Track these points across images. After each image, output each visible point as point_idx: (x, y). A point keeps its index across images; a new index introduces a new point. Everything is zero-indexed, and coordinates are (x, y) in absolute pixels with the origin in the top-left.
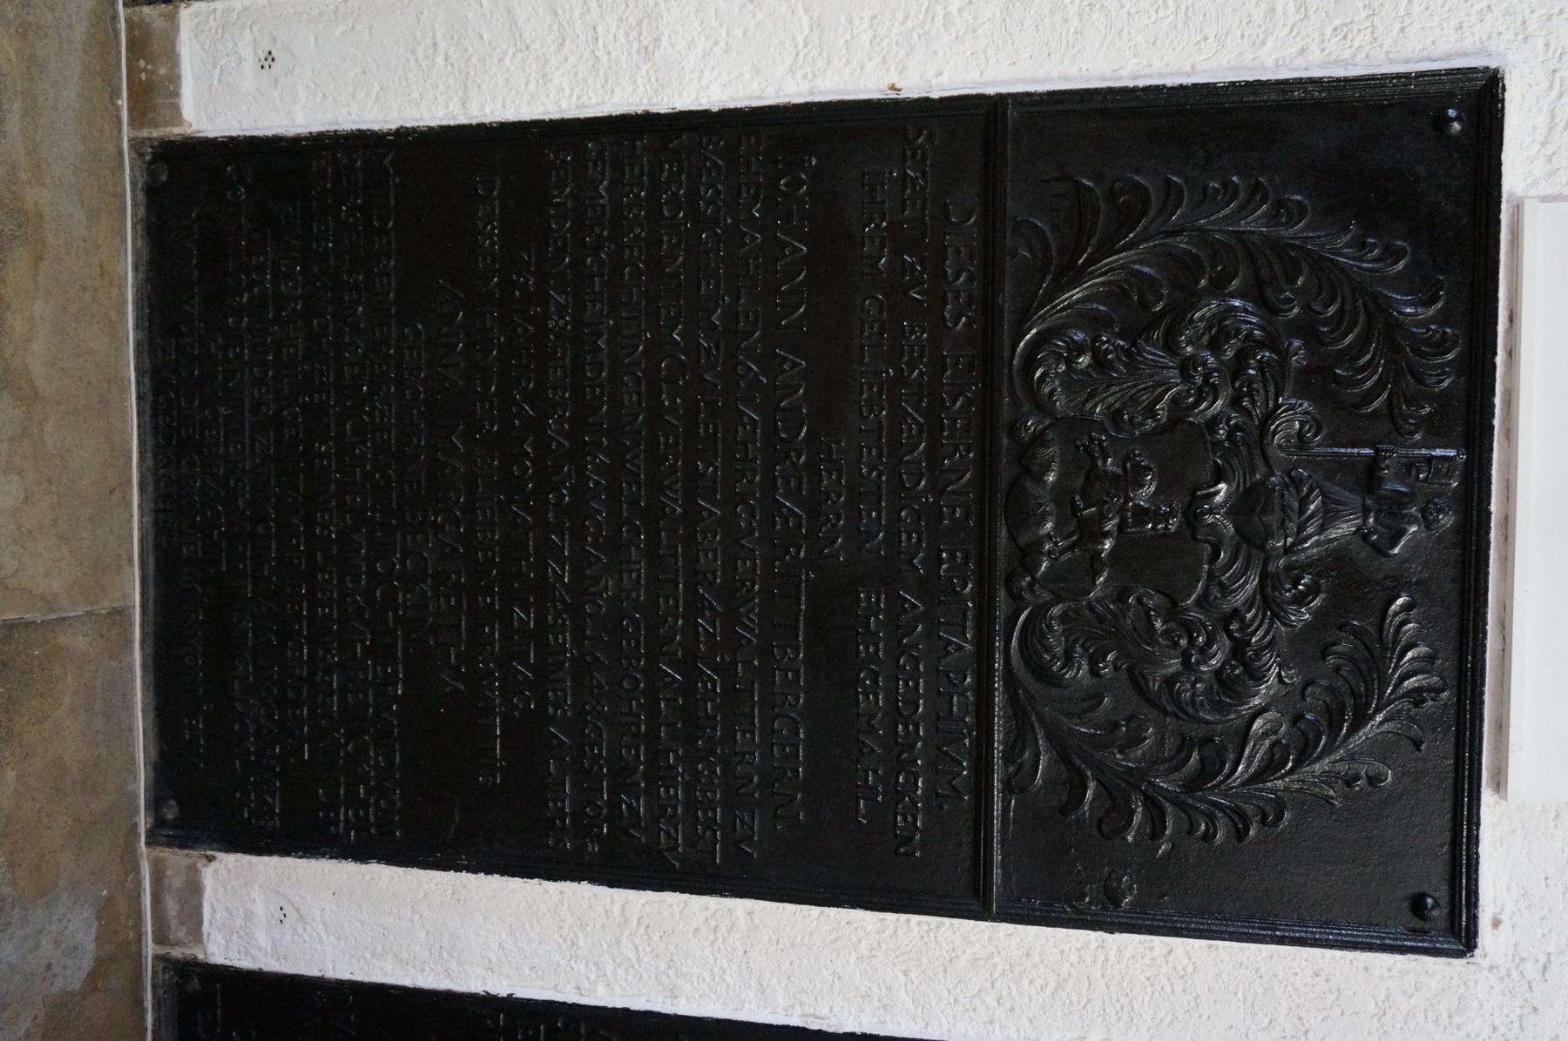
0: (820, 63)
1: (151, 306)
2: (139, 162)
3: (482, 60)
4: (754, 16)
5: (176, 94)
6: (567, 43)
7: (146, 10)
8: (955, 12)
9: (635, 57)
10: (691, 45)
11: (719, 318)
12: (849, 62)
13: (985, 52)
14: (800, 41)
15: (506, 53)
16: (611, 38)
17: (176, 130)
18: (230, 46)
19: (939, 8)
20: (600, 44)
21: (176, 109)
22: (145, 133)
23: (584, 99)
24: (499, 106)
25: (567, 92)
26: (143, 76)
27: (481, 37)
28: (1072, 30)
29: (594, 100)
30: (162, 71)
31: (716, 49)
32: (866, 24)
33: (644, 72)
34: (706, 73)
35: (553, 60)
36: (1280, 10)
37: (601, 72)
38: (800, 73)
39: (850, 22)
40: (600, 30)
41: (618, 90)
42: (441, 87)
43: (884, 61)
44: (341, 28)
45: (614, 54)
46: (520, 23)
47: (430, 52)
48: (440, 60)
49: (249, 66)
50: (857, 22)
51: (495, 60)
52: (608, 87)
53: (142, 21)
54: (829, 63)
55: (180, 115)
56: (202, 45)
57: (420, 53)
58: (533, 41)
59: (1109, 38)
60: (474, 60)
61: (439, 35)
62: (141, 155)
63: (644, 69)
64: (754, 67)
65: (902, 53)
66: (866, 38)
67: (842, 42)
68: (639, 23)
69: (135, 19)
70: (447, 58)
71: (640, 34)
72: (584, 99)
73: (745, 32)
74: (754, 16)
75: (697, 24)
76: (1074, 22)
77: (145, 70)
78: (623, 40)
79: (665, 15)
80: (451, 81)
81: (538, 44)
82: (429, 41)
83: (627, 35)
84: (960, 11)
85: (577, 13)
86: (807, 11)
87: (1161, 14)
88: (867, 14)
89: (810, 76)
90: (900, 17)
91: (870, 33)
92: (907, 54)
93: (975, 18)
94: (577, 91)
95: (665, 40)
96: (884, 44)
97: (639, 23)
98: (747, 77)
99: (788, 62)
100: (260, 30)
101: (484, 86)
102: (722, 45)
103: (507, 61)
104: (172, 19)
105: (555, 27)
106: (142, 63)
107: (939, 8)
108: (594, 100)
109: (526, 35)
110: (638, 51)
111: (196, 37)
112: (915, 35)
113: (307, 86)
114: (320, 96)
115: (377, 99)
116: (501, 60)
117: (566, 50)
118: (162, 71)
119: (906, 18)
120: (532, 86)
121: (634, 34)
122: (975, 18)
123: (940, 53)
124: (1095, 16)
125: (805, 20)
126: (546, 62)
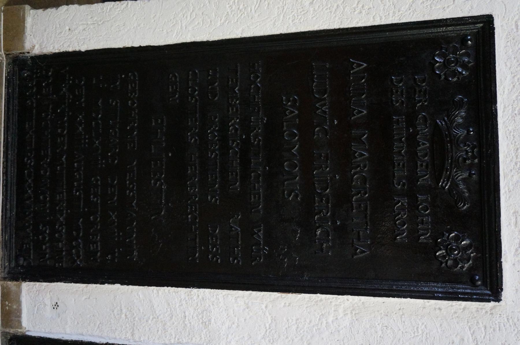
0: (276, 336)
1: (21, 336)
2: (5, 340)
3: (140, 319)
4: (249, 314)
5: (20, 316)
6: (174, 317)
7: (9, 283)
8: (331, 323)
9: (201, 326)
10: (223, 323)
11: (238, 90)
12: (287, 338)
13: (343, 341)
14: (267, 325)
15: (149, 318)
16: (191, 317)
17: (20, 330)
18: (41, 299)
19: (324, 320)
20: (187, 319)
21: (20, 322)
22: (7, 330)
23: (181, 340)
24: (147, 338)
25: (174, 336)
26: (7, 308)
27: (140, 310)
28: (379, 336)
29: (184, 341)
30: (15, 307)
31: (233, 326)
32: (294, 322)
33: (204, 333)
34: (230, 336)
35: (168, 324)
36: (466, 340)
37: (187, 330)
38: (267, 339)
39: (288, 320)
40: (187, 314)
41: (194, 339)
42: (124, 327)
43: (302, 339)
44: (85, 297)
45: (192, 323)
46: (155, 307)
47: (120, 312)
48: (123, 316)
49: (49, 308)
50: (290, 321)
51: (145, 320)
52: (190, 337)
53: (7, 286)
54: (279, 336)
55: (21, 325)
56: (31, 297)
57: (115, 311)
58: (160, 315)
59: (394, 342)
60: (137, 319)
61: (123, 306)
62: (6, 338)
63: (204, 331)
64: (249, 334)
65: (309, 337)
66: (294, 327)
67: (284, 328)
68: (202, 312)
69: (5, 286)
70: (126, 316)
71: (203, 317)
72: (181, 340)
73: (245, 320)
74: (249, 314)
75: (225, 315)
76: (380, 333)
77: (8, 306)
78: (196, 318)
79: (213, 311)
80: (128, 325)
81: (162, 316)
82: (119, 308)
83: (197, 316)
84: (332, 322)
85: (177, 305)
86: (270, 314)
87: (416, 334)
88: (294, 318)
89: (272, 341)
90: (308, 321)
91: (296, 326)
92: (311, 338)
93: (339, 326)
94: (177, 336)
95: (213, 321)
96: (301, 332)
97: (202, 312)
98: (246, 339)
99: (263, 334)
100: (53, 294)
101: (140, 330)
102: (236, 324)
103: (150, 321)
104: (19, 287)
105: (169, 310)
106: (7, 303)
107: (324, 320)
108: (184, 341)
109: (157, 312)
110: (202, 323)
111: (28, 294)
112: (314, 329)
113: (71, 318)
114: (76, 323)
115: (98, 327)
116: (147, 321)
117: (173, 320)
118: (15, 307)
119: (310, 322)
120: (160, 332)
121: (200, 316)
122: (339, 326)
123: (325, 339)
124: (388, 332)
125: (269, 318)
126: (165, 324)
